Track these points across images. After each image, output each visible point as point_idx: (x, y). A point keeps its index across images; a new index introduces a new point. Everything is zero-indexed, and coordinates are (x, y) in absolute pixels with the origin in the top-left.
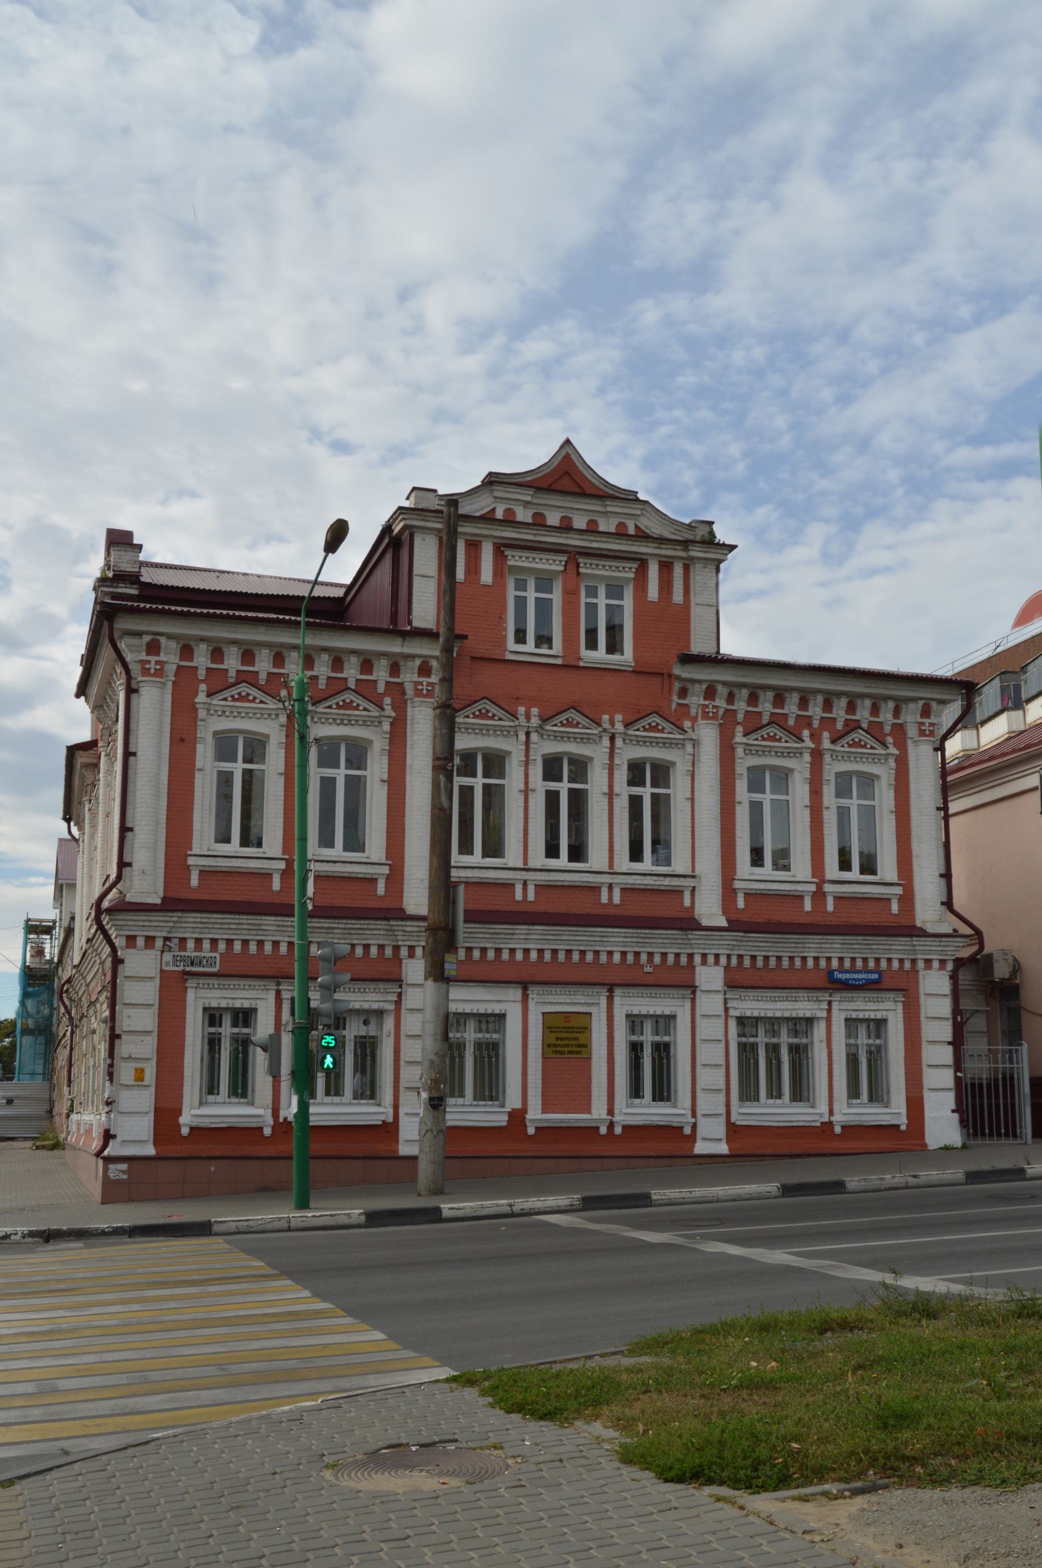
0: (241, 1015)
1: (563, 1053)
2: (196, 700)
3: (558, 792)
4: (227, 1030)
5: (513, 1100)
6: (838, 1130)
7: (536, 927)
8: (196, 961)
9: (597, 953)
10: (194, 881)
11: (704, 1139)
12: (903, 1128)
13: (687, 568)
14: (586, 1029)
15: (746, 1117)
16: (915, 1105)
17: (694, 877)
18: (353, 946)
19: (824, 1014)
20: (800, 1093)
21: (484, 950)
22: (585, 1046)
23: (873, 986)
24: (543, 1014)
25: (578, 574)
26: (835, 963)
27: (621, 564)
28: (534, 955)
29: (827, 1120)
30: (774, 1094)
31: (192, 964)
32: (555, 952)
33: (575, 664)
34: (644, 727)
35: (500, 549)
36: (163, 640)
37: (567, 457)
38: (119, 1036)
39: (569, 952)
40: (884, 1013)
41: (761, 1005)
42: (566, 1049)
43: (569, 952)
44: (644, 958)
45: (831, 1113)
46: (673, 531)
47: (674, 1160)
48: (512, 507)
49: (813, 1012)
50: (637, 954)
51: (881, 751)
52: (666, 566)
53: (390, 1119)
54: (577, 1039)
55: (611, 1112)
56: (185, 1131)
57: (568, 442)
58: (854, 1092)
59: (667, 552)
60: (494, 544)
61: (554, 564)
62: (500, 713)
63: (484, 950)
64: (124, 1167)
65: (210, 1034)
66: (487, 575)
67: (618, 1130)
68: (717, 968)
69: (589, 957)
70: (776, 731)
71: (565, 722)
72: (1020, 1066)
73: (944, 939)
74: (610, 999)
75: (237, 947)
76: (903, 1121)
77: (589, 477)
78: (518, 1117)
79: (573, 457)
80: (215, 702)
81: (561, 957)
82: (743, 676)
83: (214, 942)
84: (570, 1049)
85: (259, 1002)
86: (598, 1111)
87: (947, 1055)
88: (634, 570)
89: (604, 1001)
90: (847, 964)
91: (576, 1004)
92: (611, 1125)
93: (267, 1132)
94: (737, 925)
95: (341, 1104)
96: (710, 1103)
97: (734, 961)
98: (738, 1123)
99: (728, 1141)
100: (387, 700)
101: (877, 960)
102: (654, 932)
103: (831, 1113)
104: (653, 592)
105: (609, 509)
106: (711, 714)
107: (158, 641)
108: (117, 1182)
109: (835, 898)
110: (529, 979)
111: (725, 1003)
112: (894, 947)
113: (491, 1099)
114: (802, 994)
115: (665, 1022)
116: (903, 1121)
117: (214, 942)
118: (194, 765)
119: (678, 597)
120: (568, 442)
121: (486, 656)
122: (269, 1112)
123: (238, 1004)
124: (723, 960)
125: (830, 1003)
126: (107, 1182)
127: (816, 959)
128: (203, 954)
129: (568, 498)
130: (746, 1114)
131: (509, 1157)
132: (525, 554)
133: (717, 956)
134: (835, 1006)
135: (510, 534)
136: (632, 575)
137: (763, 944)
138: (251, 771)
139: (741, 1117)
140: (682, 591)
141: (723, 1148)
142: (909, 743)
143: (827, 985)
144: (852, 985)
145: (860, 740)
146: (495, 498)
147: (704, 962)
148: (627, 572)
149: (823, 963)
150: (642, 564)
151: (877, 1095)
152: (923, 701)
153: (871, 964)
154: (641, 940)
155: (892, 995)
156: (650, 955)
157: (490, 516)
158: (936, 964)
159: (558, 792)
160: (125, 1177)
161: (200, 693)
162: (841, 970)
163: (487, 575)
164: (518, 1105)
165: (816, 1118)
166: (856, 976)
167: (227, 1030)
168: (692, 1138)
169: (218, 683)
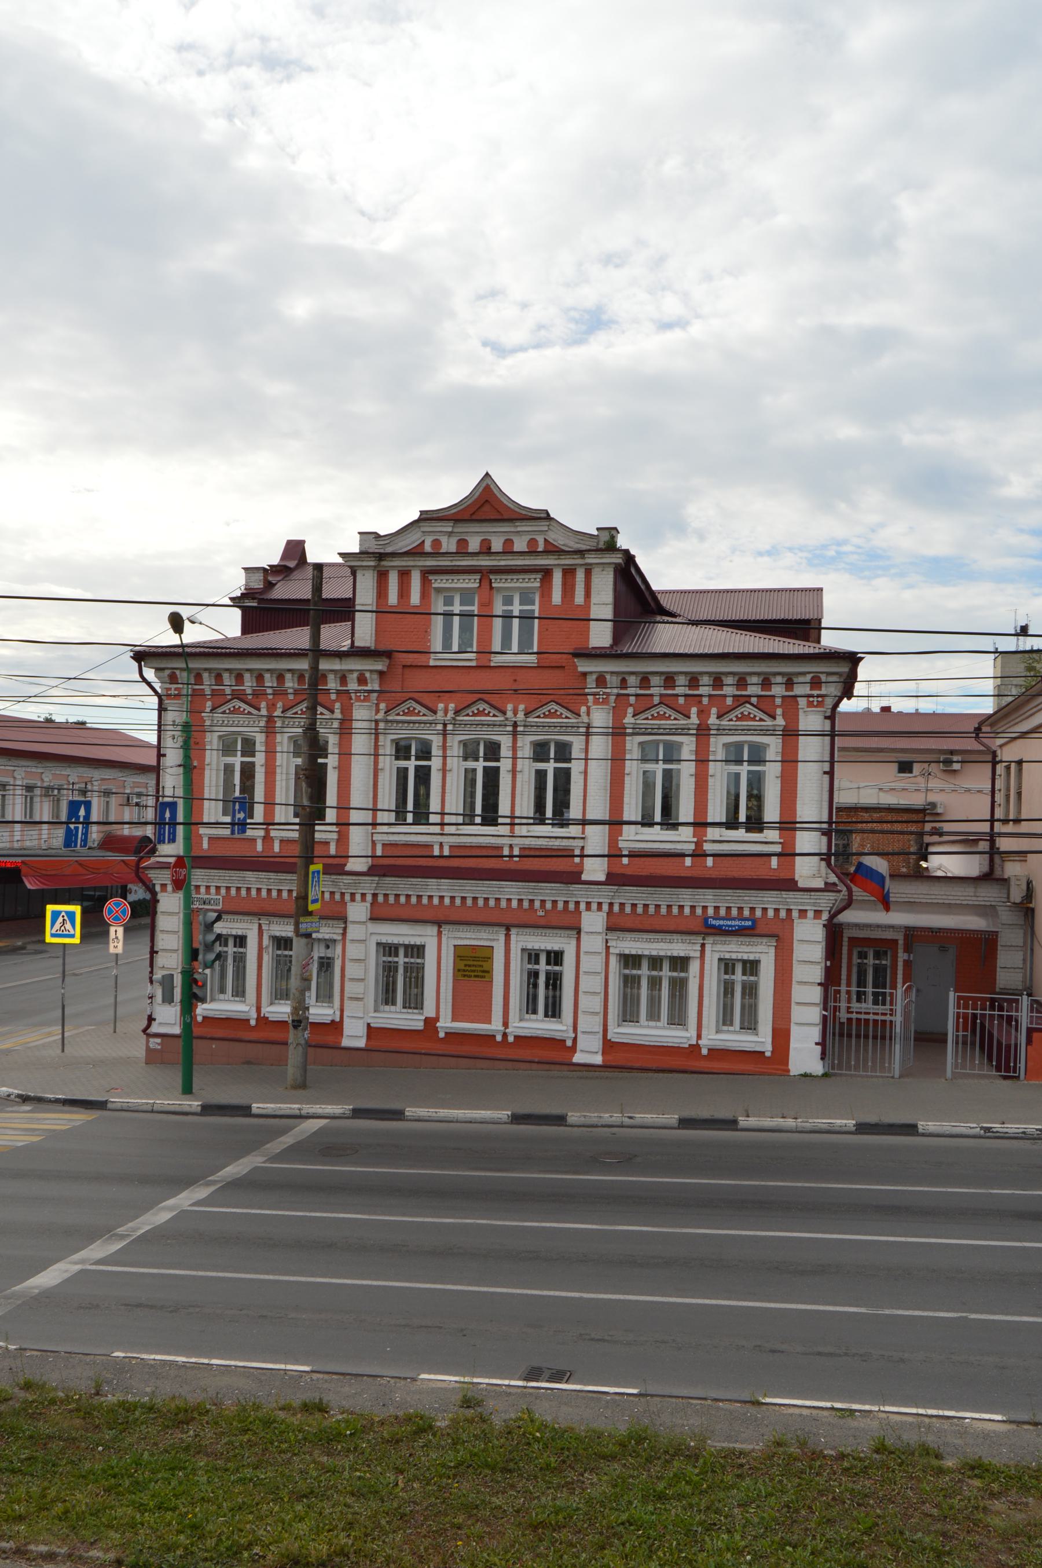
0: (552, 955)
1: (470, 976)
2: (624, 721)
3: (546, 771)
4: (738, 977)
5: (429, 1011)
6: (705, 1052)
7: (443, 881)
8: (207, 902)
9: (498, 900)
10: (205, 845)
11: (582, 1051)
12: (768, 1054)
13: (588, 573)
14: (489, 958)
15: (620, 1036)
16: (781, 1036)
17: (583, 838)
18: (323, 892)
19: (698, 954)
20: (677, 1018)
21: (408, 896)
22: (488, 972)
23: (749, 931)
24: (455, 946)
25: (491, 588)
26: (711, 912)
27: (527, 576)
28: (447, 901)
29: (695, 1043)
30: (550, 1013)
31: (204, 903)
32: (464, 899)
33: (488, 664)
34: (544, 713)
35: (427, 574)
36: (178, 672)
37: (488, 487)
38: (157, 952)
39: (475, 899)
40: (244, 931)
41: (638, 945)
42: (473, 974)
43: (475, 899)
44: (537, 904)
45: (699, 1037)
46: (577, 540)
47: (553, 1066)
48: (489, 538)
49: (687, 952)
50: (532, 901)
51: (769, 722)
52: (569, 573)
53: (338, 1020)
54: (481, 966)
55: (506, 1024)
56: (200, 1019)
57: (487, 474)
58: (726, 1018)
59: (568, 561)
60: (421, 571)
61: (471, 582)
62: (566, 713)
63: (408, 896)
64: (159, 1040)
65: (405, 963)
66: (415, 599)
67: (511, 1039)
68: (600, 913)
69: (492, 903)
70: (556, 708)
71: (547, 713)
72: (956, 1010)
73: (813, 894)
74: (508, 936)
75: (233, 892)
76: (768, 1048)
77: (505, 502)
78: (430, 1023)
79: (492, 486)
80: (723, 723)
81: (469, 902)
82: (627, 666)
83: (218, 888)
84: (476, 974)
85: (247, 931)
86: (495, 1026)
87: (815, 994)
88: (538, 580)
89: (502, 938)
90: (723, 912)
91: (481, 939)
92: (505, 1035)
93: (253, 1023)
94: (614, 879)
95: (656, 1027)
96: (590, 1023)
97: (616, 908)
98: (613, 1040)
99: (603, 1054)
100: (337, 705)
101: (753, 909)
102: (540, 884)
103: (699, 1037)
104: (557, 597)
105: (519, 529)
106: (601, 700)
107: (819, 677)
108: (155, 1050)
109: (450, 846)
110: (442, 918)
111: (607, 941)
112: (766, 899)
113: (416, 1008)
114: (675, 937)
115: (556, 957)
116: (768, 1048)
117: (218, 888)
118: (708, 771)
119: (579, 598)
120: (487, 474)
121: (413, 664)
122: (254, 1009)
123: (654, 953)
124: (605, 907)
125: (703, 945)
126: (149, 1050)
127: (693, 908)
128: (211, 897)
129: (484, 524)
130: (623, 1033)
131: (421, 1054)
132: (445, 577)
133: (600, 904)
134: (708, 948)
135: (430, 562)
136: (538, 585)
137: (640, 895)
138: (671, 770)
139: (616, 1036)
140: (583, 593)
141: (598, 1059)
142: (801, 712)
143: (704, 930)
144: (725, 931)
145: (750, 713)
146: (423, 532)
147: (353, 900)
148: (534, 582)
149: (699, 911)
150: (546, 573)
151: (750, 1024)
152: (812, 675)
153: (746, 913)
154: (531, 891)
155: (765, 940)
156: (543, 902)
157: (419, 551)
158: (810, 914)
159: (546, 771)
160: (159, 1047)
161: (628, 715)
162: (716, 917)
163: (415, 599)
164: (433, 1014)
165: (685, 1040)
166: (729, 923)
167: (738, 977)
168: (573, 1049)
169: (219, 700)
